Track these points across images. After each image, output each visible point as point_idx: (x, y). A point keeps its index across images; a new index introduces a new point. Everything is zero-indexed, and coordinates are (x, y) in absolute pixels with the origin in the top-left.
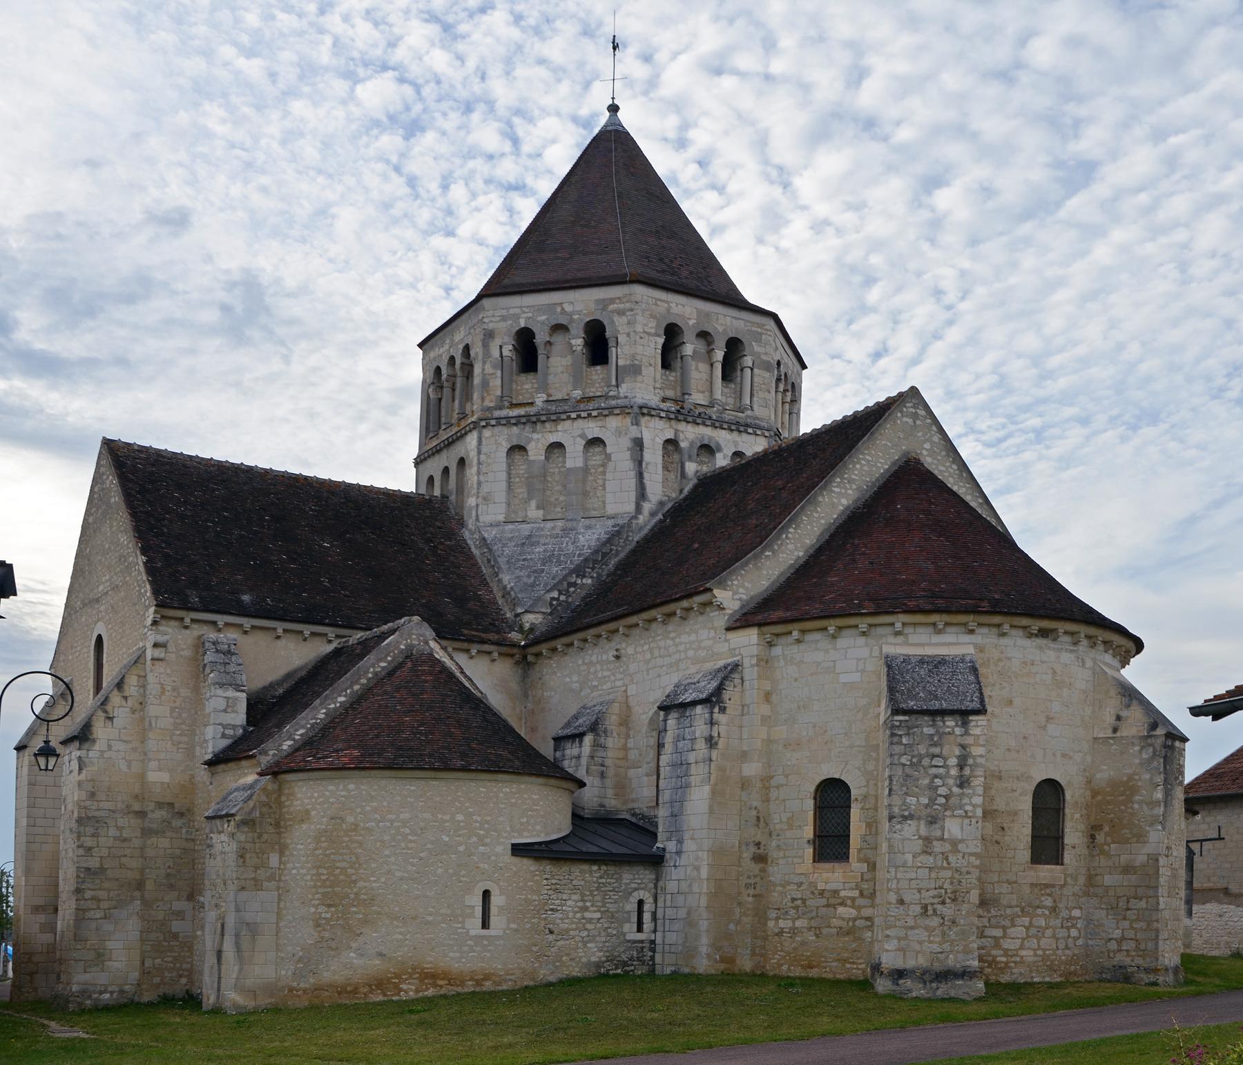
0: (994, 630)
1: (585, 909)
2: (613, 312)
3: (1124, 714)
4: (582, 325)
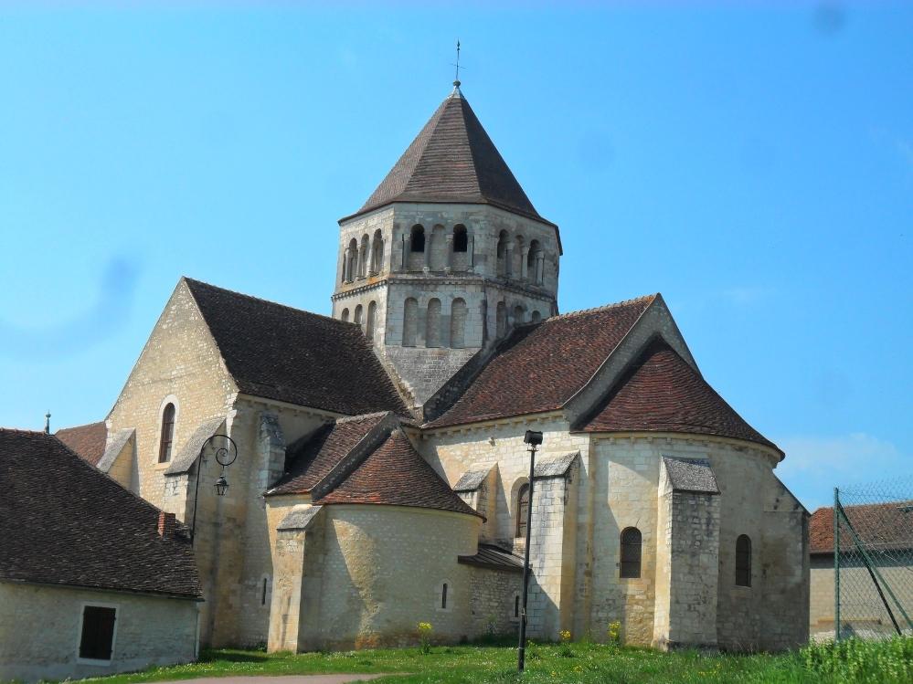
0: (717, 445)
1: (490, 600)
2: (472, 220)
3: (780, 498)
4: (453, 227)
